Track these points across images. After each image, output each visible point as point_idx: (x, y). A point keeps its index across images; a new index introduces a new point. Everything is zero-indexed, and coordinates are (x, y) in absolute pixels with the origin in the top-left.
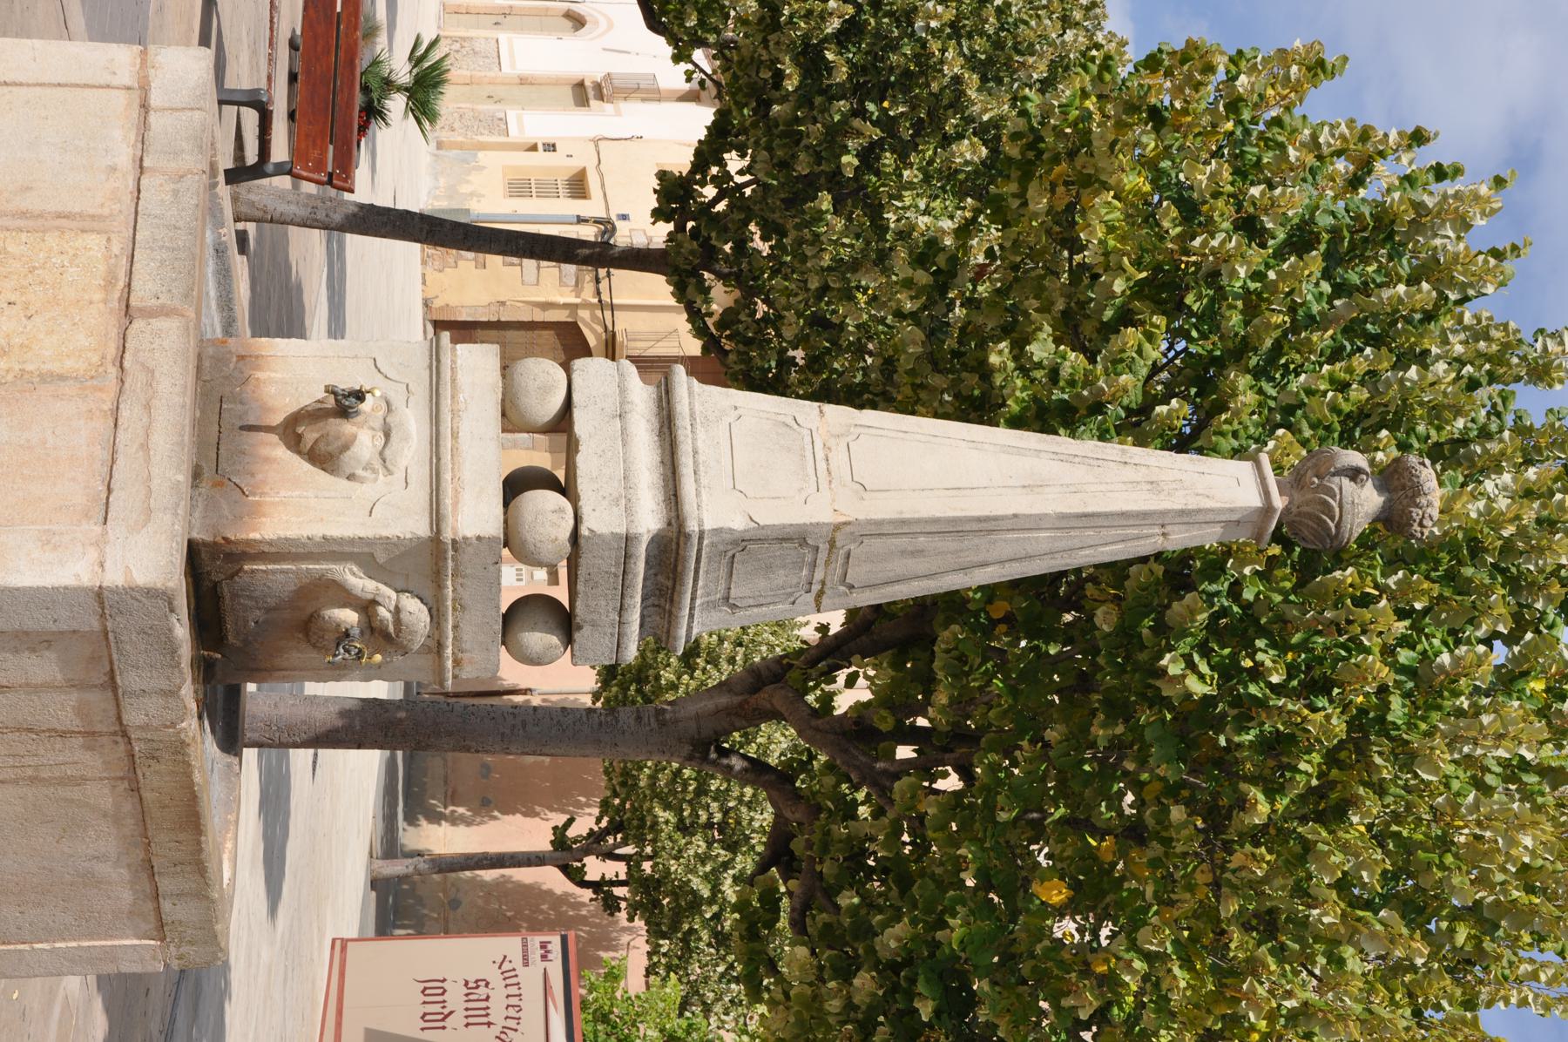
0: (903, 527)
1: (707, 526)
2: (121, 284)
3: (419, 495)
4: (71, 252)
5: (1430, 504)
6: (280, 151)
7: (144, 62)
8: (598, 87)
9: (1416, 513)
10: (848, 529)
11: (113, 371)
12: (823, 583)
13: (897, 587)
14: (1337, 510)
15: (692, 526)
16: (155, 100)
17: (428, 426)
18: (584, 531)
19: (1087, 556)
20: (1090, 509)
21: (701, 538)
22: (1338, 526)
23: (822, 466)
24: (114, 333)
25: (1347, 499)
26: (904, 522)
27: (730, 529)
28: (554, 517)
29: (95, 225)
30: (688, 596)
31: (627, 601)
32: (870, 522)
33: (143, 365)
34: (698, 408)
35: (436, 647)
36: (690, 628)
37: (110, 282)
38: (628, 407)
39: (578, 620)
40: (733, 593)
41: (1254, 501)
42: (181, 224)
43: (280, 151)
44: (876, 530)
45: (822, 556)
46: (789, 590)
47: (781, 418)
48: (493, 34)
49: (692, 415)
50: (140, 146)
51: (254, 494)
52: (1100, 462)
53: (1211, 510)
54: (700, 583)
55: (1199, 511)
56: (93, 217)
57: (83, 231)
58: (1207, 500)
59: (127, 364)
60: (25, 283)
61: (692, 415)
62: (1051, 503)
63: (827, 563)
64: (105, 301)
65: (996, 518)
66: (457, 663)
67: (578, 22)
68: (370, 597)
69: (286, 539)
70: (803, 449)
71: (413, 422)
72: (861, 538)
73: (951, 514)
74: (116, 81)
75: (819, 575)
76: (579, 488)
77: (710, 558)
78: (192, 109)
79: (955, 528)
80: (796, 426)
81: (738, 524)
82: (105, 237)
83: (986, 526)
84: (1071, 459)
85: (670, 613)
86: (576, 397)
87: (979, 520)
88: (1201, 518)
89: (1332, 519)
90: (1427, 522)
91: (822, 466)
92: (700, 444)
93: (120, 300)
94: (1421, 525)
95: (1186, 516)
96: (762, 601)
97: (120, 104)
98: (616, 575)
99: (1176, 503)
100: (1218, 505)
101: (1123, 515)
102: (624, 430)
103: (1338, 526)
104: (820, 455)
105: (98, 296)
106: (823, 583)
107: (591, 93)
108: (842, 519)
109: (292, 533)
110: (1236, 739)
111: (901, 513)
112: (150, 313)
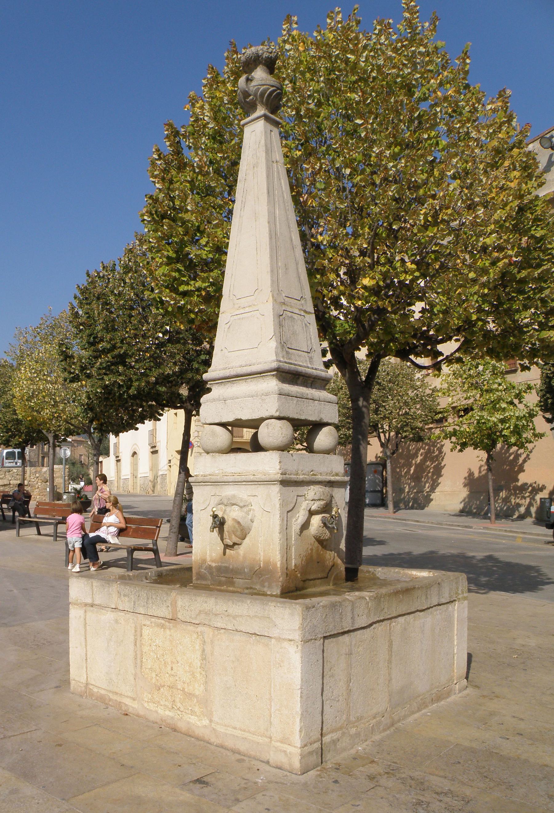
0: (274, 271)
1: (274, 358)
2: (163, 622)
3: (261, 490)
4: (150, 641)
5: (262, 49)
6: (149, 542)
7: (75, 604)
8: (152, 447)
9: (265, 55)
10: (275, 295)
11: (200, 629)
12: (301, 310)
13: (302, 278)
14: (265, 87)
15: (274, 365)
16: (89, 601)
17: (229, 486)
18: (277, 414)
19: (287, 195)
20: (265, 191)
21: (280, 361)
22: (273, 86)
23: (247, 310)
24: (183, 626)
25: (260, 83)
26: (272, 271)
27: (276, 348)
28: (270, 428)
29: (139, 630)
30: (307, 369)
31: (309, 397)
32: (272, 286)
33: (197, 615)
34: (222, 367)
35: (331, 484)
36: (321, 370)
37: (162, 626)
38: (221, 398)
39: (318, 420)
40: (306, 350)
41: (261, 123)
42: (137, 594)
43: (149, 542)
44: (275, 283)
45: (289, 309)
46: (304, 325)
47: (226, 330)
48: (138, 479)
49: (225, 369)
50: (107, 609)
51: (260, 564)
52: (245, 190)
53: (265, 140)
54: (301, 364)
55: (266, 146)
56: (136, 631)
57: (141, 636)
58: (261, 143)
59: (197, 622)
60: (163, 662)
61: (225, 369)
62: (263, 208)
63: (291, 307)
64: (170, 629)
65: (270, 231)
66: (337, 475)
67: (135, 453)
68: (307, 512)
69: (280, 550)
70: (239, 319)
71: (229, 491)
72: (279, 292)
73: (268, 251)
74: (83, 616)
75: (297, 311)
76: (257, 418)
77: (289, 359)
78: (92, 586)
79: (274, 250)
80: (230, 323)
81: (273, 344)
82: (143, 627)
83: (273, 236)
84: (243, 203)
85: (314, 378)
86: (217, 421)
87: (271, 238)
88: (269, 146)
89: (269, 89)
90: (270, 50)
91: (247, 310)
92: (237, 365)
93: (169, 623)
94: (271, 53)
95: (268, 151)
96: (309, 338)
97: (92, 616)
98: (298, 401)
99: (263, 160)
100: (263, 137)
101: (268, 177)
102: (232, 398)
103: (273, 86)
104: (242, 311)
105: (168, 632)
106: (301, 310)
107: (154, 449)
108: (271, 298)
109: (278, 548)
110: (362, 176)
111: (268, 272)
112: (175, 612)
